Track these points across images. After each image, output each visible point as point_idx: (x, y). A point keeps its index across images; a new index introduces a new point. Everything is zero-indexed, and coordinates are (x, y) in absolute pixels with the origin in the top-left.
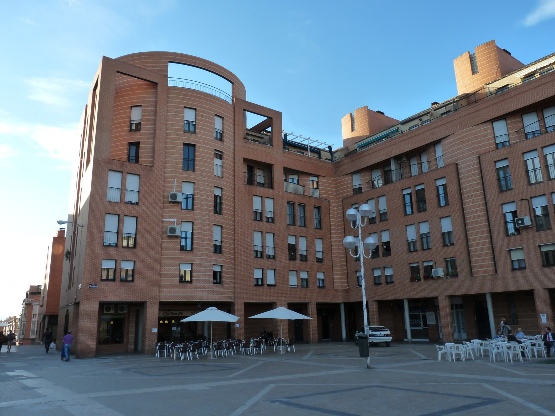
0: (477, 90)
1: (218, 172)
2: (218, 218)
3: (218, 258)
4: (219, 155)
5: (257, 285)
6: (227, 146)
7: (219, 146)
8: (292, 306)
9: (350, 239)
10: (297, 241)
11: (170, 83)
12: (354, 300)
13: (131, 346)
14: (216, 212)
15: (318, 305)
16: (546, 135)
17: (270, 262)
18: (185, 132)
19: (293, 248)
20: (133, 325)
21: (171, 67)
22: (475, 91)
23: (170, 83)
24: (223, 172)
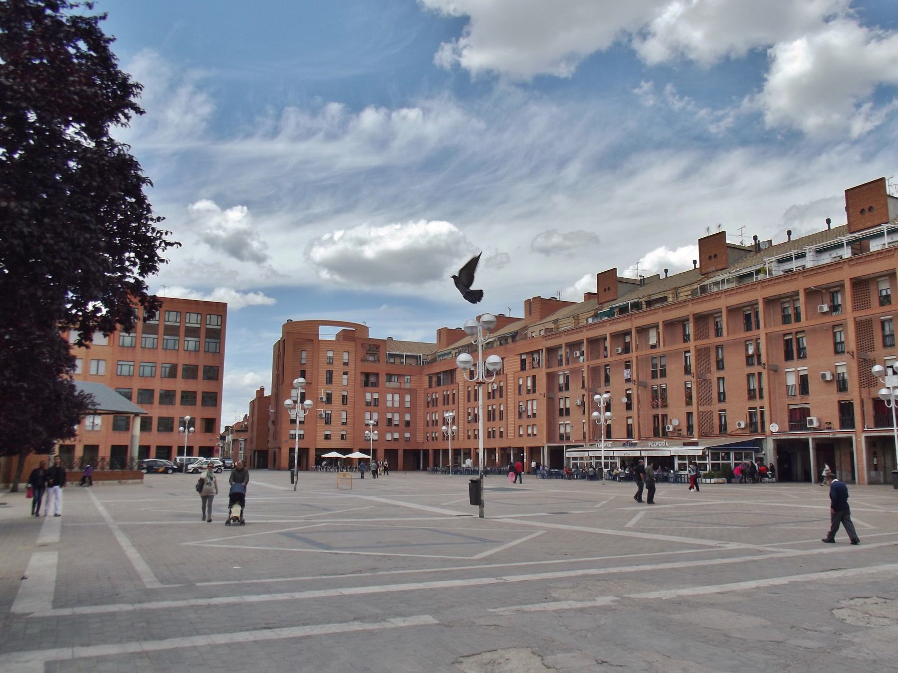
0: (714, 311)
1: (345, 382)
2: (345, 407)
3: (344, 427)
4: (345, 373)
5: (406, 441)
6: (351, 368)
7: (346, 368)
8: (361, 451)
9: (595, 414)
10: (393, 416)
11: (320, 338)
12: (446, 448)
13: (305, 468)
14: (343, 404)
15: (405, 450)
16: (896, 337)
17: (396, 428)
18: (328, 363)
19: (390, 421)
20: (305, 458)
21: (322, 329)
22: (710, 312)
23: (320, 338)
24: (348, 382)
